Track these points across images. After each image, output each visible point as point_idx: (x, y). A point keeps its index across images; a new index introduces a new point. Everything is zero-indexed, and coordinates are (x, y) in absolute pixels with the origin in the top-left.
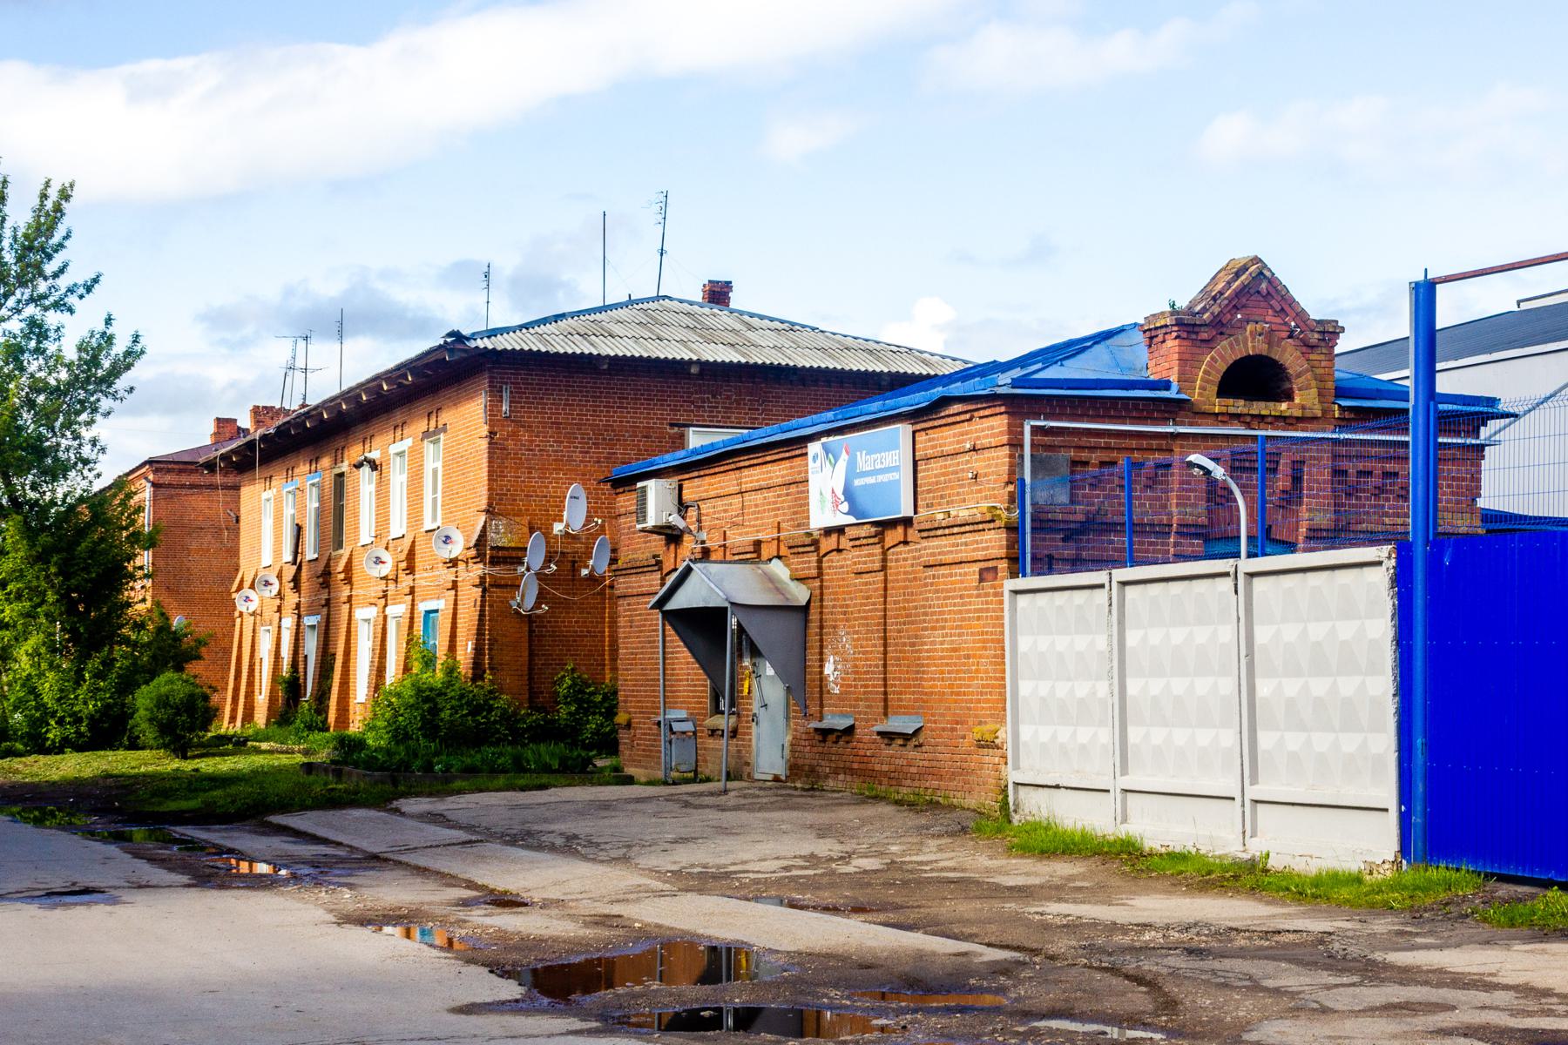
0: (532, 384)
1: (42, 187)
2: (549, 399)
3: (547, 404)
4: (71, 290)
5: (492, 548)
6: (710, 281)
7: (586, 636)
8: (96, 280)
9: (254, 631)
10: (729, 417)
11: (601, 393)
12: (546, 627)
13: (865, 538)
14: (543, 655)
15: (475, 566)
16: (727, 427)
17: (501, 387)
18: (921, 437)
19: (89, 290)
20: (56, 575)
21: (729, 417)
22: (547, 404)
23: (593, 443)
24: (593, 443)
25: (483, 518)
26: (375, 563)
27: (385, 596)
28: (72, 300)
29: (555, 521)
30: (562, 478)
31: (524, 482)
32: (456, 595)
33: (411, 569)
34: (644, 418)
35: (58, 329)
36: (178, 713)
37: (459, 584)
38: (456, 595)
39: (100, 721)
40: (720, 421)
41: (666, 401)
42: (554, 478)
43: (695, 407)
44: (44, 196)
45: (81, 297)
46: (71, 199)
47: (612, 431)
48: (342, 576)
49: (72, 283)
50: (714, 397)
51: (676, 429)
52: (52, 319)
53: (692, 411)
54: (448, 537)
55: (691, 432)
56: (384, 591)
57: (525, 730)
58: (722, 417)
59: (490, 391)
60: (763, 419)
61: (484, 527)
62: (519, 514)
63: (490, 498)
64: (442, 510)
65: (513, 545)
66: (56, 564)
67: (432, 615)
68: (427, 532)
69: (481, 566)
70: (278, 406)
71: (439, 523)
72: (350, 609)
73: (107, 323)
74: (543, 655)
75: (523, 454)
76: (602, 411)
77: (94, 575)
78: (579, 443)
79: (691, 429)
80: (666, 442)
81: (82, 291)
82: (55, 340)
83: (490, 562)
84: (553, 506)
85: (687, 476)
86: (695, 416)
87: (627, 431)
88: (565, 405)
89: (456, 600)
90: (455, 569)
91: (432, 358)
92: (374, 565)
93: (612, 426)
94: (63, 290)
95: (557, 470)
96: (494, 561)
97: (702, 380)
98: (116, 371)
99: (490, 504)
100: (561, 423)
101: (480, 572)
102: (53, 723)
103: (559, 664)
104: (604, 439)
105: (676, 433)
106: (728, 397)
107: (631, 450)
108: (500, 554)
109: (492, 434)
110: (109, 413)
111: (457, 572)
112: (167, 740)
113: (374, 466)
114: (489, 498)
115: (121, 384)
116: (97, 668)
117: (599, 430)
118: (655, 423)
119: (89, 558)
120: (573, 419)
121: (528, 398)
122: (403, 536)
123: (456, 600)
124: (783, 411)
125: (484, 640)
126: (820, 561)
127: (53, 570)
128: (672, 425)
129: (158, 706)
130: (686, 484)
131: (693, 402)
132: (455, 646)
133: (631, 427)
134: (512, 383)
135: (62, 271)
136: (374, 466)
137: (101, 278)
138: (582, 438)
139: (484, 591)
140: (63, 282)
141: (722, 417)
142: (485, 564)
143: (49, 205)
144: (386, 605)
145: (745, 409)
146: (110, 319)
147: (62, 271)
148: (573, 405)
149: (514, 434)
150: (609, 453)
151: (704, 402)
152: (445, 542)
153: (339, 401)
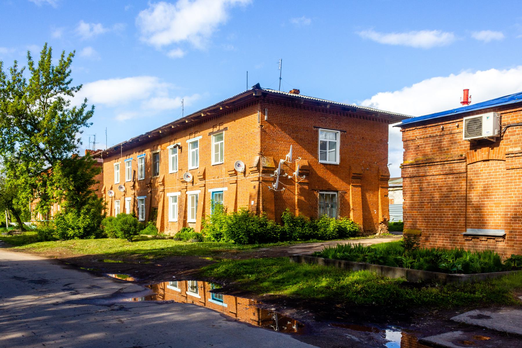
0: (274, 109)
1: (62, 53)
2: (279, 115)
3: (278, 117)
4: (72, 89)
5: (263, 167)
6: (294, 89)
7: (290, 199)
8: (81, 87)
9: (112, 202)
10: (330, 126)
11: (294, 114)
12: (278, 196)
13: (457, 160)
14: (277, 206)
15: (161, 187)
16: (330, 129)
17: (265, 109)
18: (503, 116)
19: (79, 89)
20: (72, 181)
21: (330, 126)
22: (278, 117)
23: (292, 132)
24: (292, 132)
25: (258, 158)
26: (187, 177)
27: (186, 188)
28: (73, 92)
29: (281, 158)
30: (282, 144)
31: (271, 144)
32: (237, 185)
33: (204, 178)
34: (307, 124)
35: (68, 102)
36: (130, 226)
37: (238, 181)
38: (237, 185)
39: (86, 228)
40: (327, 127)
41: (313, 118)
42: (280, 143)
43: (321, 121)
44: (63, 56)
45: (76, 92)
46: (74, 56)
47: (298, 128)
48: (103, 192)
49: (73, 87)
50: (326, 118)
51: (315, 129)
52: (66, 97)
53: (320, 123)
54: (239, 164)
55: (320, 130)
56: (186, 187)
57: (279, 232)
58: (328, 126)
59: (261, 110)
60: (339, 127)
61: (259, 160)
62: (270, 155)
63: (261, 149)
64: (200, 162)
65: (270, 166)
66: (71, 177)
67: (214, 193)
68: (213, 166)
69: (258, 173)
70: (92, 150)
71: (198, 167)
72: (164, 193)
73: (85, 101)
74: (277, 206)
75: (271, 134)
76: (294, 121)
77: (83, 182)
78: (288, 131)
79: (320, 129)
80: (313, 133)
81: (76, 89)
82: (67, 105)
83: (262, 172)
84: (280, 153)
85: (503, 112)
86: (321, 124)
87: (301, 128)
88: (284, 117)
89: (237, 187)
90: (236, 176)
91: (196, 115)
92: (186, 178)
93: (297, 126)
94: (70, 89)
95: (281, 141)
96: (264, 172)
97: (323, 112)
98: (86, 118)
99: (261, 152)
100: (282, 124)
101: (258, 176)
102: (71, 229)
103: (282, 209)
104: (295, 131)
105: (315, 130)
106: (330, 119)
107: (303, 135)
108: (266, 170)
109: (261, 126)
110: (82, 132)
111: (237, 177)
112: (126, 235)
113: (180, 148)
114: (261, 149)
115: (88, 121)
116: (85, 212)
117: (294, 127)
118: (310, 126)
119: (81, 176)
120: (286, 123)
121: (273, 114)
122: (198, 168)
123: (237, 187)
124: (345, 125)
125: (260, 200)
126: (467, 166)
127: (71, 179)
128: (314, 127)
129: (123, 224)
130: (503, 116)
131: (320, 120)
132: (237, 203)
133: (302, 127)
134: (268, 108)
135: (69, 83)
136: (180, 148)
137: (82, 86)
138: (289, 130)
139: (260, 183)
140: (70, 86)
141: (328, 126)
142: (260, 173)
143: (65, 59)
144: (187, 191)
145: (334, 123)
146: (86, 100)
147: (69, 83)
148: (286, 118)
149: (268, 127)
150: (296, 136)
151: (323, 120)
152: (238, 166)
153: (170, 125)
